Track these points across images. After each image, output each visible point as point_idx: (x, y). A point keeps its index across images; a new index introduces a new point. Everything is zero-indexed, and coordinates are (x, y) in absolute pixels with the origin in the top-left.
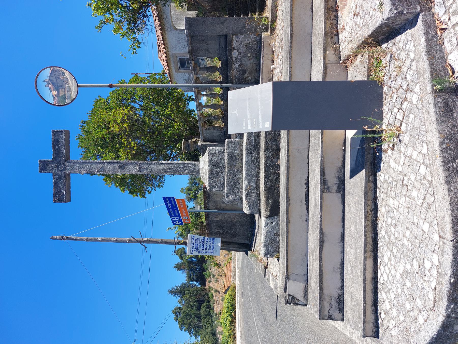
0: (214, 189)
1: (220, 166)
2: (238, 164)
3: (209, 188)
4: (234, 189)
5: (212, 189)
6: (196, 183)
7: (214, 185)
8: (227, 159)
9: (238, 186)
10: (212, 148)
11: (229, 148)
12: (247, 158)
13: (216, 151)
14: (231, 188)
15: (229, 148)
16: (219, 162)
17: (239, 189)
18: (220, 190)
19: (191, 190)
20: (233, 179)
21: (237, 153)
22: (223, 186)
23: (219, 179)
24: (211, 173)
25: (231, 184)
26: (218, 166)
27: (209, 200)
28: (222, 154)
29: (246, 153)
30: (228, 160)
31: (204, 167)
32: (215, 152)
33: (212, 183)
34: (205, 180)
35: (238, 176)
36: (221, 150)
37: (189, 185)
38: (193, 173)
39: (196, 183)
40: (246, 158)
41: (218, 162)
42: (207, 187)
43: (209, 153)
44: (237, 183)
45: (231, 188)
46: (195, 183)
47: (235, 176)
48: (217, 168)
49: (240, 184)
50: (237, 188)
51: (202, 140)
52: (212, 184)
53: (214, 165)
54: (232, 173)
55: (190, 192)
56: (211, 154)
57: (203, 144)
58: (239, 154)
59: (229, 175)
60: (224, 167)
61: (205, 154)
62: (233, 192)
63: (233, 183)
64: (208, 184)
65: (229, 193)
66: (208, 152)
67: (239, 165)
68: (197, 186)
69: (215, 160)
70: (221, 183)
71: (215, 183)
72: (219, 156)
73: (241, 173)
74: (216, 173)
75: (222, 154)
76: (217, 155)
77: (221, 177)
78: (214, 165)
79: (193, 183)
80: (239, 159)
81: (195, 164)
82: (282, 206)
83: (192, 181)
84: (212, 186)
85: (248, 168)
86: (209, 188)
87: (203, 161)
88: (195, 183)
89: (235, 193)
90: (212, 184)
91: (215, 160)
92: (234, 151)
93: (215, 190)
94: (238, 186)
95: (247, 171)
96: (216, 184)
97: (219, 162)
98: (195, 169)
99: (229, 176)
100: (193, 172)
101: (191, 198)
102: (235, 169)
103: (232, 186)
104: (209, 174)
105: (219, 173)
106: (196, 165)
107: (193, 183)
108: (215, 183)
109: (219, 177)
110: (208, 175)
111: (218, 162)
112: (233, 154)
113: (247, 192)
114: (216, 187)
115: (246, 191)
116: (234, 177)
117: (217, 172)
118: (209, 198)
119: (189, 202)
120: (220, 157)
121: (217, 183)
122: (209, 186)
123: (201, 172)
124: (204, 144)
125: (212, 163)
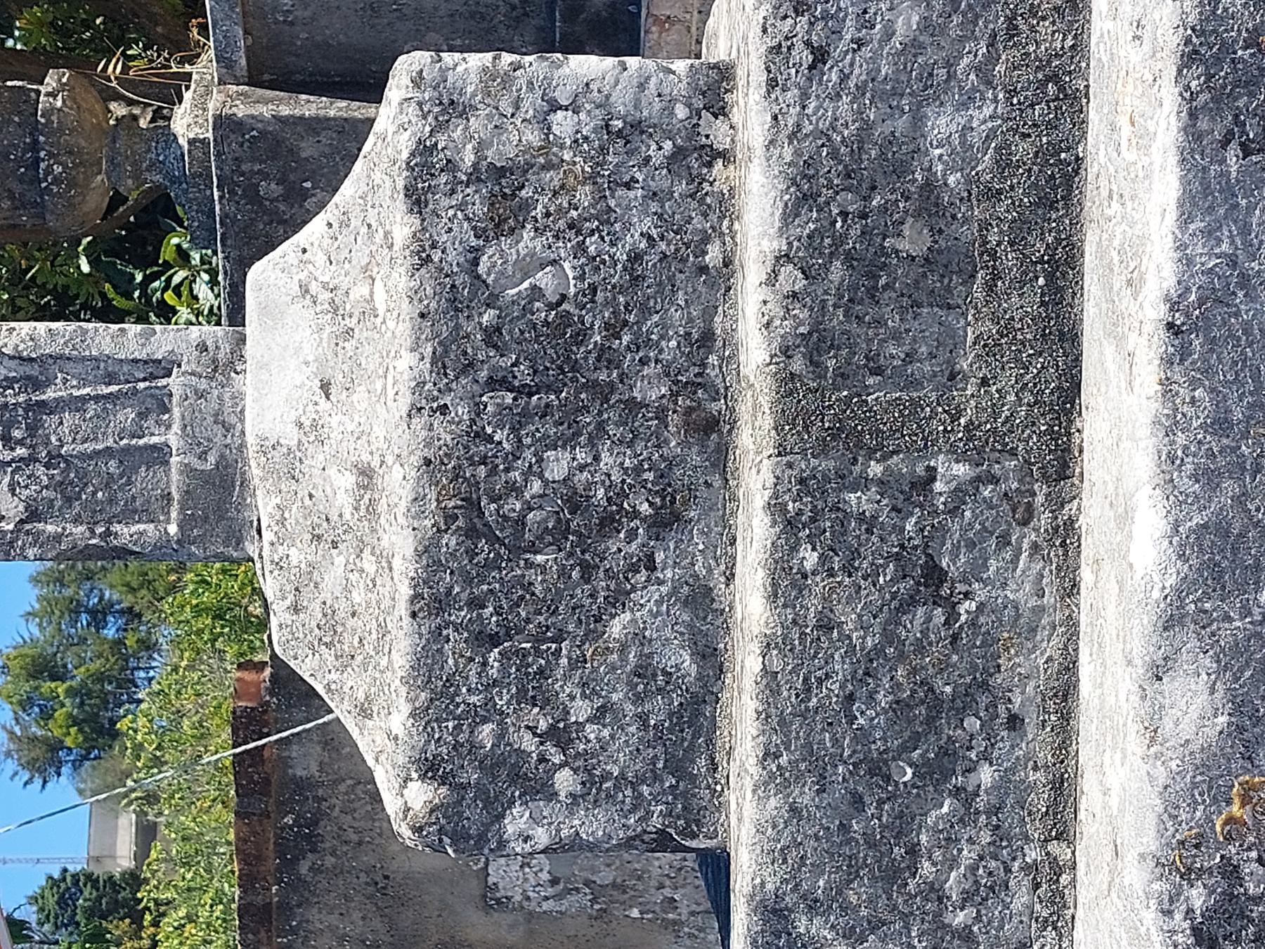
0: (516, 821)
1: (633, 406)
2: (989, 349)
3: (420, 795)
4: (903, 826)
5: (474, 815)
6: (99, 616)
7: (528, 743)
8: (783, 258)
9: (986, 775)
10: (477, 60)
11: (820, 56)
12: (1210, 233)
13: (563, 123)
14: (857, 802)
15: (820, 56)
16: (613, 330)
17: (1009, 819)
18: (628, 843)
19: (58, 675)
20: (889, 637)
21: (964, 155)
22: (678, 767)
23: (617, 627)
24: (471, 533)
25: (862, 736)
26: (604, 393)
27: (304, 868)
28: (662, 181)
29: (1192, 133)
30: (791, 278)
31: (335, 423)
32: (533, 137)
33: (488, 712)
34: (345, 661)
35: (976, 572)
36: (651, 109)
37: (36, 631)
38: (125, 533)
39: (99, 616)
40: (1185, 220)
41: (595, 322)
42: (384, 779)
43: (424, 150)
44: (963, 703)
45: (857, 802)
46: (92, 612)
47: (934, 575)
48: (568, 442)
49: (1014, 722)
50: (966, 797)
51: (223, 59)
52: (486, 733)
53: (523, 374)
54: (869, 523)
55: (47, 686)
56: (475, 177)
57: (241, 111)
58: (1004, 164)
59: (810, 558)
60: (711, 425)
61: (348, 190)
62: (892, 876)
63: (900, 707)
64: (399, 720)
65: (813, 906)
66: (404, 145)
67: (1007, 379)
68: (110, 632)
69: (544, 279)
70: (658, 709)
71: (544, 700)
72: (606, 217)
73: (1044, 519)
74: (563, 530)
75: (662, 181)
76: (584, 196)
77: (647, 598)
78: (523, 374)
79: (75, 608)
80: (1009, 259)
81: (161, 367)
82: (263, 575)
83: (68, 592)
84: (491, 765)
85: (1220, 425)
86: (420, 795)
87: (301, 315)
88: (92, 612)
89: (935, 892)
90: (486, 733)
91: (544, 279)
92: (918, 120)
93: (542, 837)
94: (986, 775)
95: (1208, 478)
96: (561, 735)
97: (613, 330)
98: (159, 455)
99: (819, 584)
100: (129, 515)
101: (55, 747)
102: (928, 445)
103: (878, 770)
104: (427, 550)
105: (609, 524)
106: (175, 383)
107: (75, 608)
108: (544, 700)
109: (618, 599)
110: (405, 566)
111: (595, 322)
112: (900, 170)
113: (1197, 897)
114: (565, 781)
115: (1189, 874)
116: (911, 602)
117: (575, 501)
118: (312, 842)
119: (38, 782)
120: (633, 239)
121: (581, 710)
122: (430, 769)
123: (265, 505)
124: (266, 111)
125: (492, 336)
